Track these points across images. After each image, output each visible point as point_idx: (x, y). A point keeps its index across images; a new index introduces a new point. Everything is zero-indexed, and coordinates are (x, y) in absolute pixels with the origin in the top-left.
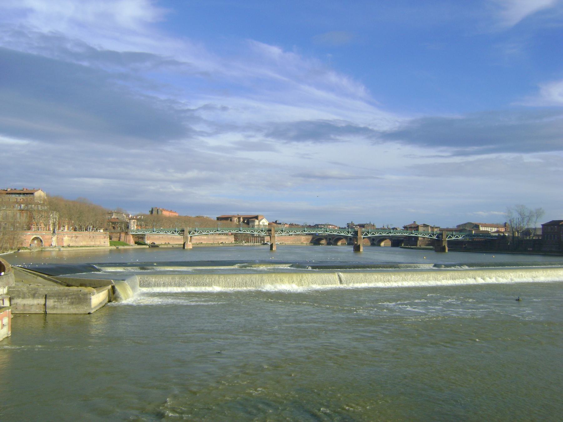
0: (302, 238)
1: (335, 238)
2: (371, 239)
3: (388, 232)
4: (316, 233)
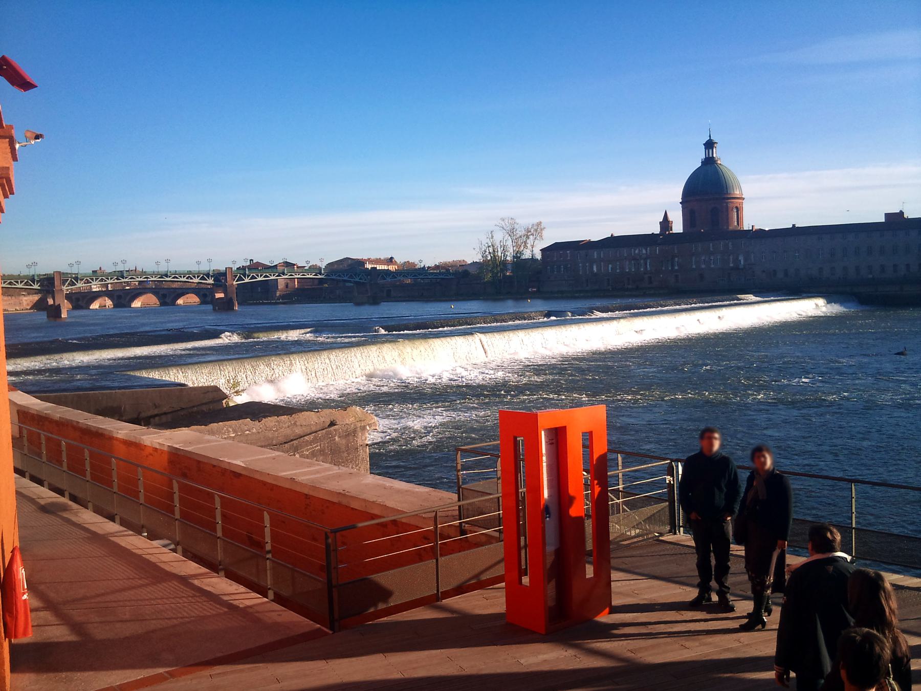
2: (160, 295)
4: (146, 280)
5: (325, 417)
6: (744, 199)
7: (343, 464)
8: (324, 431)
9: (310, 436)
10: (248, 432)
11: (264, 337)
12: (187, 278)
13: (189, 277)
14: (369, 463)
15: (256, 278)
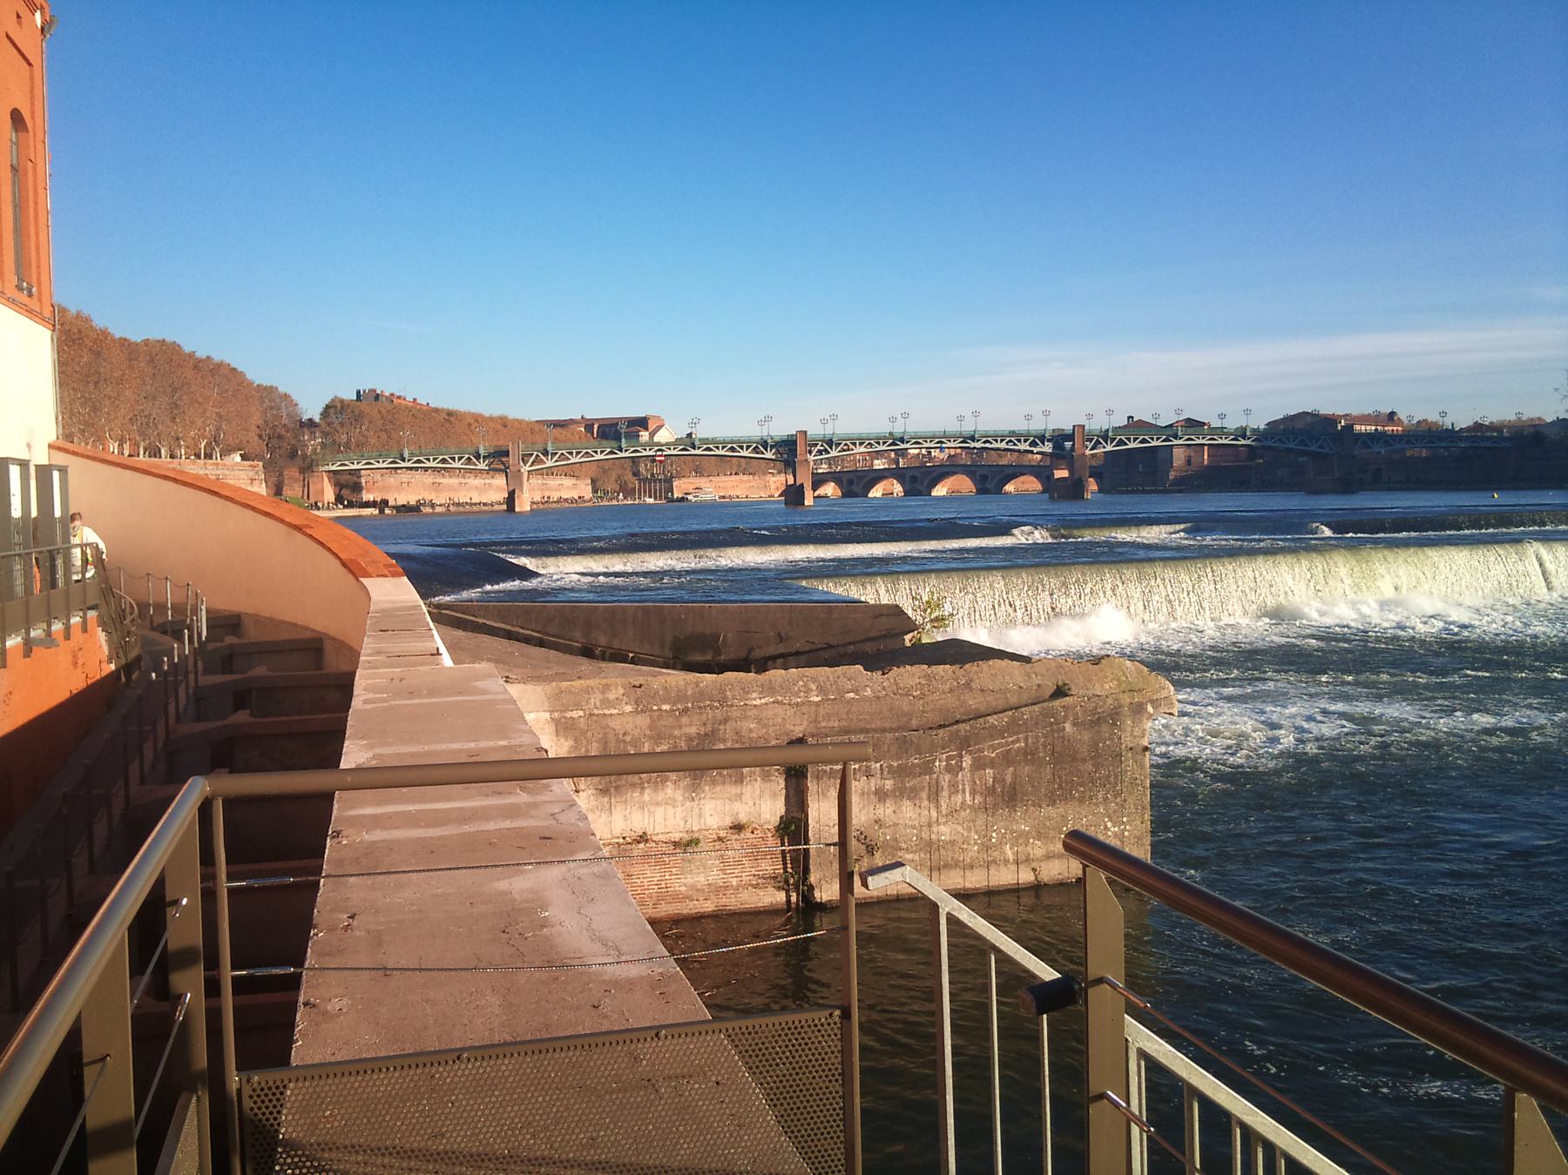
0: (771, 483)
3: (1168, 435)
5: (1043, 676)
7: (1082, 789)
8: (1036, 708)
9: (1001, 715)
10: (852, 695)
11: (1088, 536)
13: (1011, 441)
15: (1126, 444)
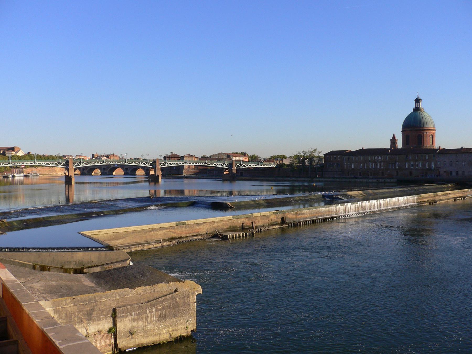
0: (57, 169)
1: (89, 168)
2: (125, 169)
6: (436, 130)
8: (170, 295)
12: (136, 164)
14: (196, 312)
